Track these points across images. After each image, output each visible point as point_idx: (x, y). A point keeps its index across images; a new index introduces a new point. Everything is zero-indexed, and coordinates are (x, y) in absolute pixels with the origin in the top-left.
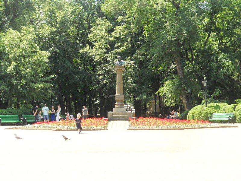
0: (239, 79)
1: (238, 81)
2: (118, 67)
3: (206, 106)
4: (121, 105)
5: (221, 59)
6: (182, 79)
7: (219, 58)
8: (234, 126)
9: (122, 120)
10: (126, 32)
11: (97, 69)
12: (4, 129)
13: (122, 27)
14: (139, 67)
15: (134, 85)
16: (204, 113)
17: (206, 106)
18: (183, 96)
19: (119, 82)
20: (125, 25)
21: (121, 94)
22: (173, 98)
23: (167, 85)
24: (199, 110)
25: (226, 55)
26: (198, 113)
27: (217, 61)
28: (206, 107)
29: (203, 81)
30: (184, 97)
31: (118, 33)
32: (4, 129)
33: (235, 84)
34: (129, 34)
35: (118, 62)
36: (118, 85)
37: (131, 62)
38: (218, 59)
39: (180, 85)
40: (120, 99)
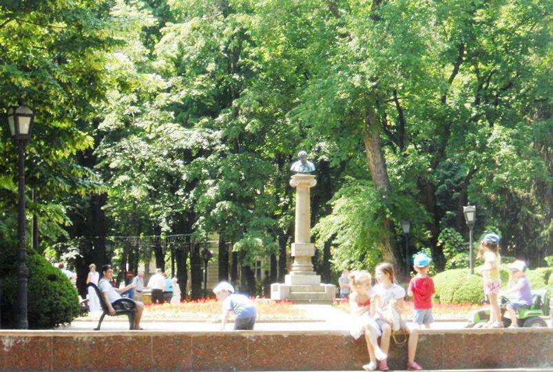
0: (531, 194)
1: (528, 199)
2: (304, 178)
3: (473, 273)
4: (307, 268)
5: (496, 141)
6: (385, 194)
7: (490, 140)
8: (121, 323)
9: (320, 304)
10: (201, 42)
11: (104, 151)
12: (324, 321)
13: (185, 28)
14: (236, 150)
15: (227, 205)
16: (468, 291)
17: (473, 273)
18: (384, 244)
19: (304, 214)
20: (196, 21)
21: (307, 242)
22: (356, 248)
23: (340, 211)
24: (454, 282)
25: (510, 131)
26: (452, 290)
27: (483, 148)
28: (474, 276)
29: (465, 208)
30: (388, 244)
31: (175, 46)
32: (324, 321)
33: (524, 209)
34: (210, 49)
35: (301, 166)
36: (300, 219)
37: (212, 136)
38: (487, 143)
39: (380, 213)
40: (304, 254)
